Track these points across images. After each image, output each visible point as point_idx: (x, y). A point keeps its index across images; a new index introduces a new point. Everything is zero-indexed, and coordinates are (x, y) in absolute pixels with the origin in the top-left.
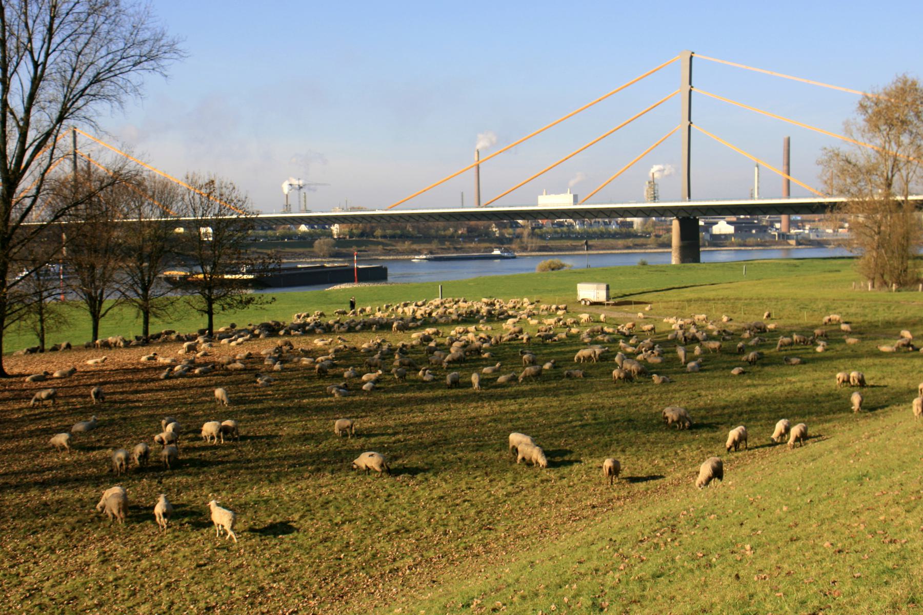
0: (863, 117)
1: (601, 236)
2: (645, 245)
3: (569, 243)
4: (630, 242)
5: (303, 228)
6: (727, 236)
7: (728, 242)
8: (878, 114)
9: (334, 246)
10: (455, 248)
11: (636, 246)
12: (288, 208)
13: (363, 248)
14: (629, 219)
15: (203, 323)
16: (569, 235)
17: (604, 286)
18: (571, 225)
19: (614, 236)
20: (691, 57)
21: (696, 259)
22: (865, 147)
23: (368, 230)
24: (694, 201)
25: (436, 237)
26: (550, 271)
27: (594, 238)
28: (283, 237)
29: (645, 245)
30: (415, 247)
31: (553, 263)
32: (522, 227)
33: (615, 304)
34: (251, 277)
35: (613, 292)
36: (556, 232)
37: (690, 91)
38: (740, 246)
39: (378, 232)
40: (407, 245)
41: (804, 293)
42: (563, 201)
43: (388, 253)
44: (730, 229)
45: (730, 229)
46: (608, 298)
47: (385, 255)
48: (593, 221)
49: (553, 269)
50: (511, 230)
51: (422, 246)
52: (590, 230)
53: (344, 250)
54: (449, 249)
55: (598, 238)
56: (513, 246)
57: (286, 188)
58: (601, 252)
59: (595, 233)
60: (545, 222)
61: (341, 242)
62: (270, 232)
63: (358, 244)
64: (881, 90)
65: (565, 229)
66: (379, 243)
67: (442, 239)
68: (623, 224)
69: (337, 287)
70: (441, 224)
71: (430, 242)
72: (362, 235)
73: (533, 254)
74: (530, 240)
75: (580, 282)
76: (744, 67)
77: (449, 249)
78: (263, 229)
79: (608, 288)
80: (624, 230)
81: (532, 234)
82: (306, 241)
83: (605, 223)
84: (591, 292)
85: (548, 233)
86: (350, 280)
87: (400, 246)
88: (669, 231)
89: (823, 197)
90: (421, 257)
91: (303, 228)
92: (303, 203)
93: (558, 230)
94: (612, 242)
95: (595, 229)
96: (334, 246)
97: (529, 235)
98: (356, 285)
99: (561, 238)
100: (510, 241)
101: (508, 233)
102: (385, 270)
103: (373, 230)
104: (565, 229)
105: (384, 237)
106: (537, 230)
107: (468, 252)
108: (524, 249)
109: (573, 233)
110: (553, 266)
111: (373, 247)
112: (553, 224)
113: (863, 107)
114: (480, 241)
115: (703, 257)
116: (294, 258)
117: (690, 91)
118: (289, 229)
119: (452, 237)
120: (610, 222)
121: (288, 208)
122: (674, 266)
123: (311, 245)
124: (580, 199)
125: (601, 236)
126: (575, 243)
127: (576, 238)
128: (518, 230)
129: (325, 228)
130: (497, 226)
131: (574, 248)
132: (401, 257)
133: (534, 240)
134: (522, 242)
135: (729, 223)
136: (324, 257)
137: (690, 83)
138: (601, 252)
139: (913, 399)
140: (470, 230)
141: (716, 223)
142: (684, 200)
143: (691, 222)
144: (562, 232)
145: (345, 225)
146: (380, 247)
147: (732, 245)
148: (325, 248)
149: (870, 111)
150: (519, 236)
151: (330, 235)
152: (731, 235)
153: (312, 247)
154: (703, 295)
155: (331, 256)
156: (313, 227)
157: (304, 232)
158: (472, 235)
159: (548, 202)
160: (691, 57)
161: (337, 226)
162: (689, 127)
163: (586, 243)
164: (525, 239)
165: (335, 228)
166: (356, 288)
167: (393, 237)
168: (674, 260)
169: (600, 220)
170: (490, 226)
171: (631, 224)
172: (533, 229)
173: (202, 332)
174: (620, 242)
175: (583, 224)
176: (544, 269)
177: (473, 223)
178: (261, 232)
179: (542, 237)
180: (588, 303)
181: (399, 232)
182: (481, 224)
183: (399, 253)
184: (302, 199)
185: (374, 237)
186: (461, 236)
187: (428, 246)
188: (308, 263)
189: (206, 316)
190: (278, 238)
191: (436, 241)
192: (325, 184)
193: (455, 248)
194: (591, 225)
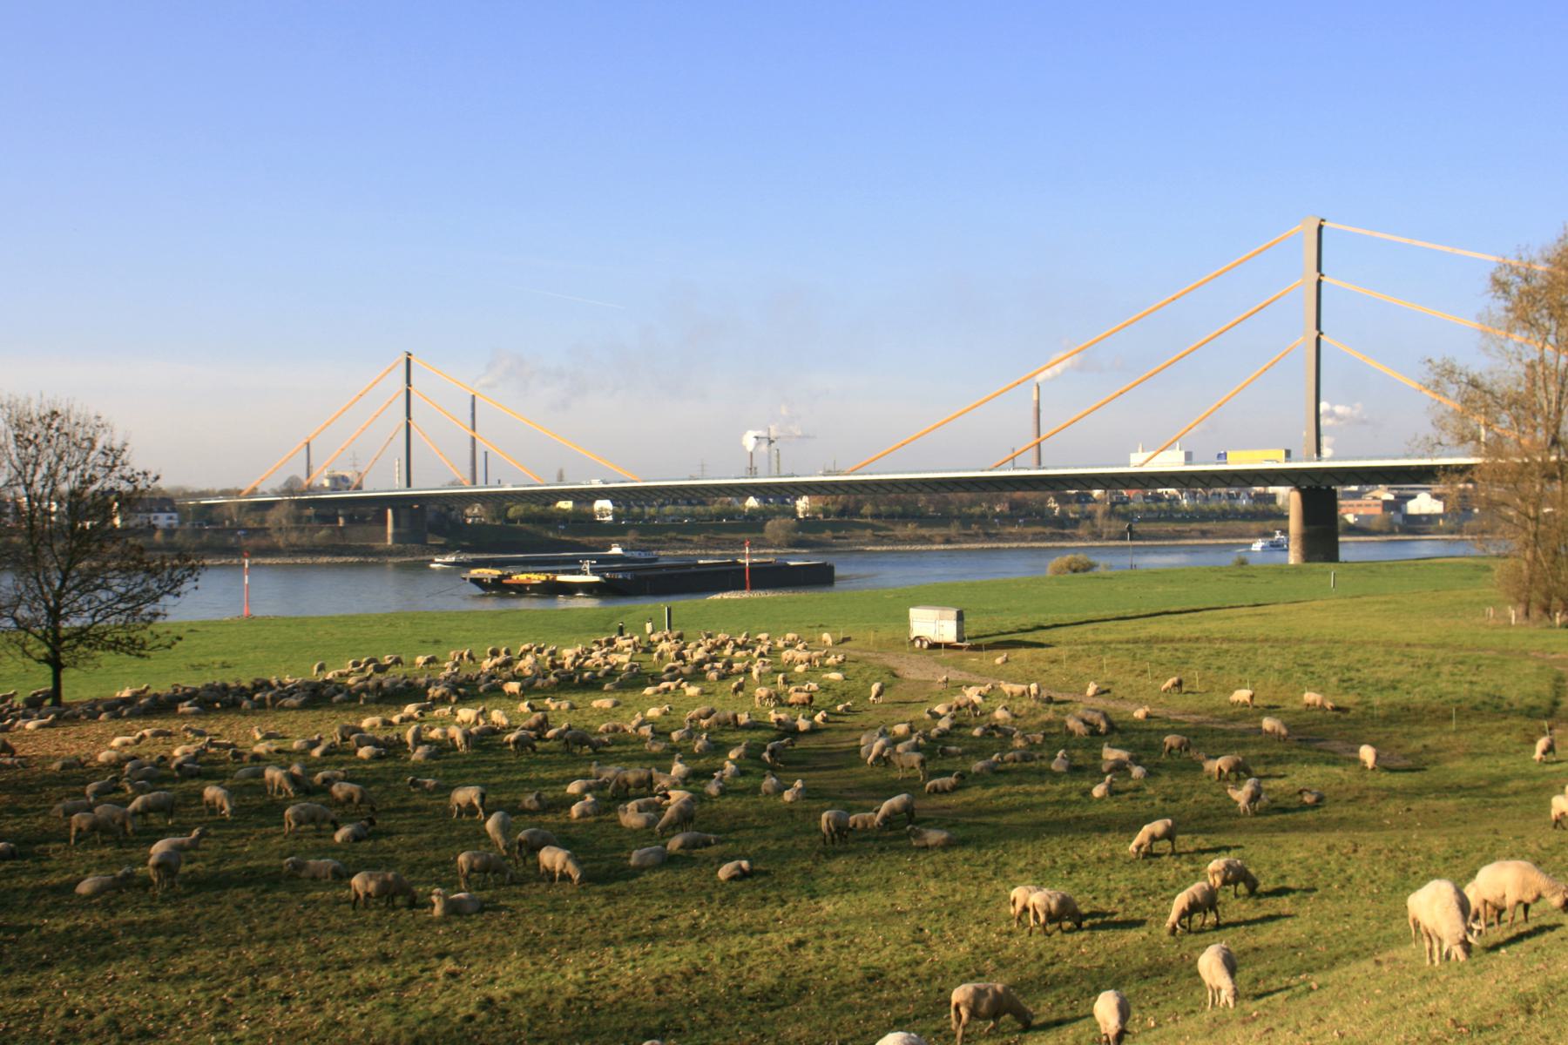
0: (1502, 303)
1: (1223, 516)
3: (1170, 527)
5: (752, 502)
6: (1431, 518)
7: (1432, 527)
8: (1530, 297)
9: (796, 530)
10: (987, 534)
12: (752, 471)
13: (843, 533)
14: (1271, 489)
15: (41, 680)
16: (1171, 513)
17: (953, 613)
18: (1175, 498)
19: (1248, 516)
20: (1320, 228)
21: (1331, 555)
22: (1505, 358)
23: (851, 506)
24: (1297, 460)
25: (958, 517)
26: (1070, 575)
27: (1211, 520)
28: (719, 517)
30: (925, 532)
31: (1076, 561)
32: (1095, 501)
33: (971, 648)
34: (596, 579)
35: (973, 627)
36: (1150, 510)
37: (1319, 282)
38: (1452, 532)
39: (867, 509)
40: (910, 529)
41: (1391, 629)
42: (1171, 461)
43: (879, 540)
44: (1437, 507)
45: (1437, 507)
46: (960, 638)
47: (875, 543)
48: (1210, 492)
49: (1075, 571)
50: (1077, 507)
51: (936, 531)
52: (1205, 507)
53: (812, 537)
54: (977, 535)
56: (1080, 532)
57: (749, 442)
58: (1222, 541)
59: (1213, 511)
60: (1133, 493)
61: (809, 524)
62: (700, 509)
63: (834, 527)
64: (1535, 255)
65: (1164, 505)
66: (865, 526)
67: (966, 520)
68: (1260, 497)
69: (718, 597)
70: (966, 496)
71: (947, 525)
72: (842, 512)
73: (1112, 543)
74: (1106, 522)
75: (914, 606)
76: (1448, 249)
77: (977, 535)
78: (689, 503)
79: (960, 617)
80: (1261, 507)
81: (1111, 514)
82: (754, 522)
83: (1230, 496)
84: (933, 624)
85: (1137, 511)
86: (739, 586)
87: (900, 531)
90: (448, 559)
91: (752, 502)
92: (774, 464)
93: (1154, 506)
94: (1240, 525)
95: (1213, 505)
96: (796, 530)
97: (1105, 514)
98: (745, 595)
99: (1158, 519)
100: (1075, 523)
101: (1073, 510)
102: (831, 568)
103: (859, 505)
104: (1164, 505)
105: (876, 516)
106: (1119, 507)
107: (1007, 541)
108: (1097, 536)
109: (1178, 511)
110: (1074, 566)
111: (858, 532)
112: (1145, 497)
113: (1501, 286)
114: (1027, 524)
115: (1343, 554)
116: (733, 548)
117: (1319, 282)
118: (729, 504)
119: (983, 516)
120: (1238, 495)
121: (752, 471)
122: (1295, 567)
123: (760, 528)
124: (1195, 458)
125: (1223, 516)
126: (1179, 527)
127: (1183, 520)
128: (1089, 507)
129: (784, 502)
130: (1057, 500)
132: (900, 548)
133: (1114, 522)
134: (1094, 525)
135: (1437, 497)
136: (779, 546)
137: (1319, 269)
138: (1222, 541)
139: (1488, 859)
140: (1014, 506)
141: (1414, 497)
142: (1309, 460)
143: (1320, 491)
144: (1160, 510)
145: (816, 498)
146: (868, 532)
147: (1440, 531)
148: (781, 533)
149: (1514, 291)
150: (1090, 517)
151: (794, 513)
152: (1437, 516)
153: (762, 531)
154: (1143, 634)
155: (790, 546)
156: (766, 501)
157: (751, 509)
158: (1019, 513)
159: (1138, 462)
160: (1320, 228)
161: (805, 499)
162: (1318, 340)
163: (1130, 528)
164: (1099, 522)
165: (802, 504)
166: (748, 600)
167: (891, 516)
168: (1293, 557)
169: (1223, 491)
170: (1044, 502)
171: (1272, 498)
172: (1113, 504)
173: (34, 703)
175: (1193, 496)
176: (1058, 571)
177: (1018, 495)
178: (685, 509)
179: (1125, 517)
180: (925, 645)
181: (899, 509)
182: (1030, 495)
183: (897, 541)
184: (774, 459)
185: (862, 516)
186: (997, 516)
187: (944, 531)
188: (714, 557)
189: (47, 670)
190: (712, 517)
191: (957, 523)
193: (987, 534)
194: (1207, 498)
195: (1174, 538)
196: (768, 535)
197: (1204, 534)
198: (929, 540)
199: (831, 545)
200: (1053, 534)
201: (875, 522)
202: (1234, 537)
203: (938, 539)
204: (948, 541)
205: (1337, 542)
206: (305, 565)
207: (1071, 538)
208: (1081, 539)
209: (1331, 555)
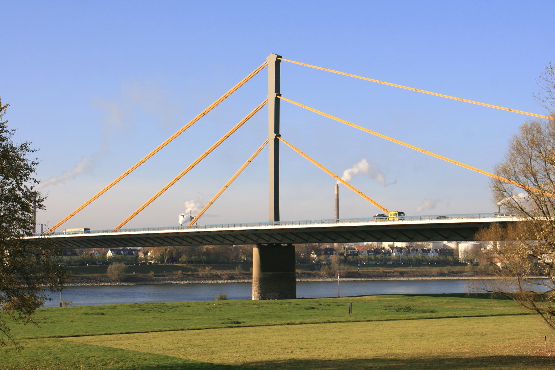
2: (462, 272)
3: (381, 270)
4: (445, 269)
11: (451, 273)
16: (382, 260)
21: (288, 293)
24: (344, 221)
29: (462, 272)
30: (219, 272)
36: (370, 259)
40: (207, 270)
47: (182, 279)
53: (141, 275)
55: (414, 265)
59: (411, 260)
71: (234, 268)
88: (251, 255)
89: (507, 215)
93: (373, 257)
94: (428, 268)
99: (376, 265)
108: (332, 275)
109: (390, 260)
115: (300, 292)
122: (255, 303)
126: (387, 270)
131: (386, 275)
134: (330, 268)
148: (116, 273)
155: (122, 281)
168: (255, 295)
174: (435, 270)
183: (199, 278)
192: (215, 216)
195: (382, 277)
196: (109, 274)
197: (402, 274)
198: (219, 277)
199: (152, 280)
200: (302, 274)
201: (188, 266)
202: (421, 276)
203: (224, 277)
204: (232, 278)
205: (295, 281)
206: (377, 281)
207: (314, 276)
208: (321, 277)
209: (288, 293)
